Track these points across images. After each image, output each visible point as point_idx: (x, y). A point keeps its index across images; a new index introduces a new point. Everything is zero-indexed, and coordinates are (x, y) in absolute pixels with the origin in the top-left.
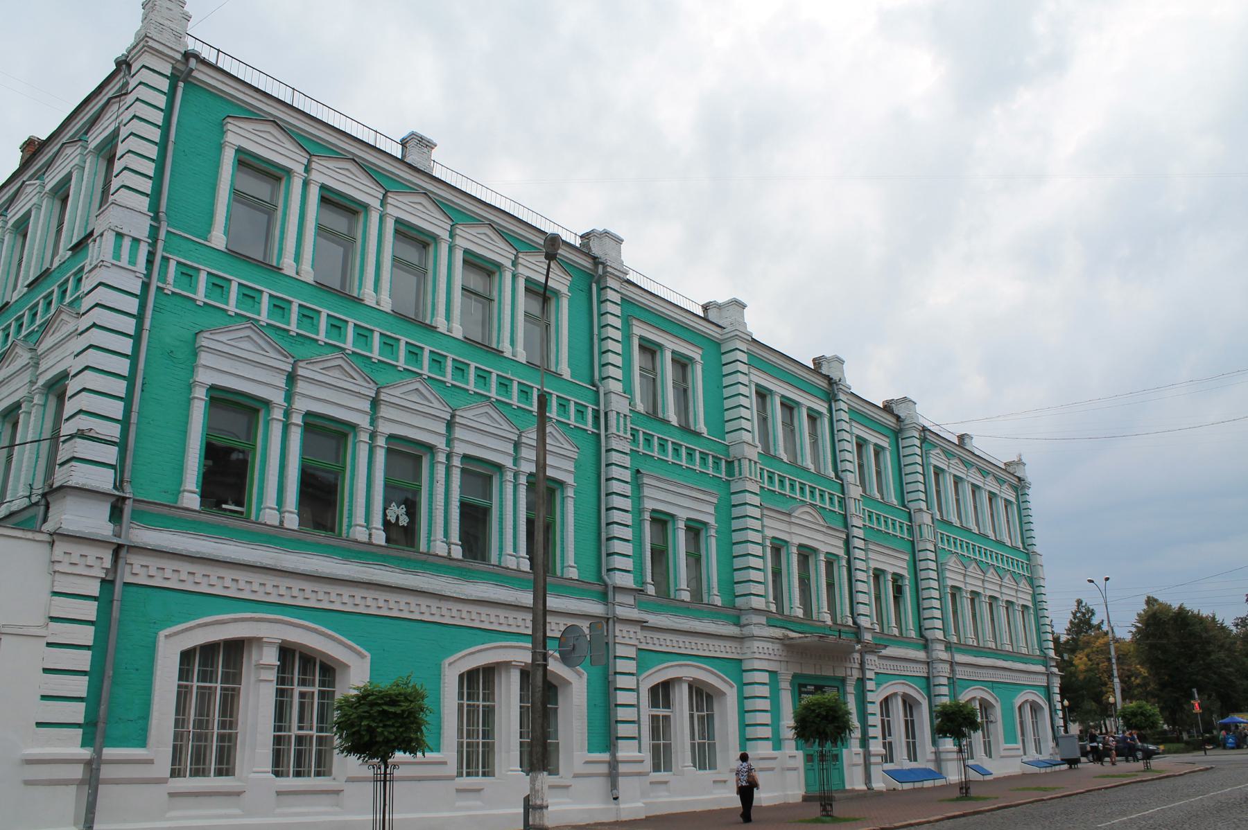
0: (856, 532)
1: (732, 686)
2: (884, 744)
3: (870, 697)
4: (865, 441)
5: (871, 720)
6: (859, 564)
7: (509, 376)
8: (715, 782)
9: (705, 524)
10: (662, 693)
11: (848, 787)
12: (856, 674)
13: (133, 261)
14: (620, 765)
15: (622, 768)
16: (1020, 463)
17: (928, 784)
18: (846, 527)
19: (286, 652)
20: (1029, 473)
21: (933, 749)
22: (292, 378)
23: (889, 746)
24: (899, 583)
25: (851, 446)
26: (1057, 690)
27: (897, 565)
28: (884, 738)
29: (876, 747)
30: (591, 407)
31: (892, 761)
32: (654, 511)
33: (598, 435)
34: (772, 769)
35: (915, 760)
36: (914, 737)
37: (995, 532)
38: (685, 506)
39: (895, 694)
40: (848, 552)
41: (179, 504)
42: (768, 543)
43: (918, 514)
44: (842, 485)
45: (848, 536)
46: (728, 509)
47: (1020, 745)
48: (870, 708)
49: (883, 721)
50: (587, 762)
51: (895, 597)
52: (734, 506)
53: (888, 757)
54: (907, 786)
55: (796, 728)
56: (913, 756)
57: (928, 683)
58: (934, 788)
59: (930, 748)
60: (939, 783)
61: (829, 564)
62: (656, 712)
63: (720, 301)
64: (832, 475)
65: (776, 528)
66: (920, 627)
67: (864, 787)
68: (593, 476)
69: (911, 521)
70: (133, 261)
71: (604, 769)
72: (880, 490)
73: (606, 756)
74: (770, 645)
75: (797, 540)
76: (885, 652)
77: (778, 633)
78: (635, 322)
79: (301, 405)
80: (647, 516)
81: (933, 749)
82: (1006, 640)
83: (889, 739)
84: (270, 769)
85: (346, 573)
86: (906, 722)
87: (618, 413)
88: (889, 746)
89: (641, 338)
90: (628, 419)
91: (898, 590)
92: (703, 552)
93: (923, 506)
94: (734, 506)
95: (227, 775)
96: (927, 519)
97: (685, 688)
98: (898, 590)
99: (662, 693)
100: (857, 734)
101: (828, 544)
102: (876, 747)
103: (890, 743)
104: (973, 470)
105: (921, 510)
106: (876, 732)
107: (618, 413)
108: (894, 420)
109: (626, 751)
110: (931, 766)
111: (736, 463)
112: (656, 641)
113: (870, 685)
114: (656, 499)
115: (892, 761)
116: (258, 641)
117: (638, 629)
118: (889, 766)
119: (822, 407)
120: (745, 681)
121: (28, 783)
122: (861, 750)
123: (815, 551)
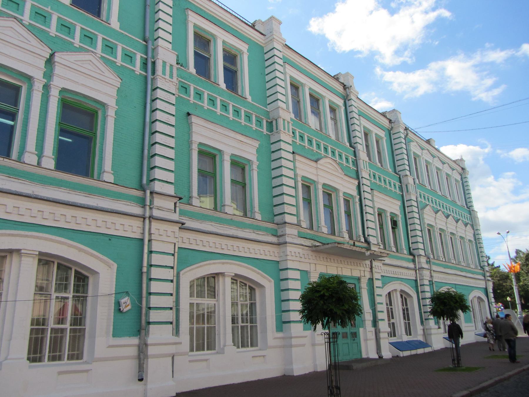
0: (365, 181)
1: (270, 281)
2: (389, 324)
3: (377, 291)
4: (370, 130)
5: (379, 308)
6: (368, 203)
7: (49, 9)
8: (253, 357)
9: (249, 161)
10: (208, 285)
11: (364, 356)
12: (368, 276)
13: (171, 76)
14: (150, 348)
15: (151, 350)
16: (462, 160)
17: (420, 351)
18: (358, 178)
19: (45, 260)
20: (467, 165)
21: (422, 328)
22: (50, 61)
23: (393, 326)
24: (395, 219)
25: (435, 171)
26: (491, 291)
27: (393, 207)
28: (389, 320)
29: (384, 326)
30: (139, 57)
31: (395, 336)
32: (200, 144)
33: (146, 77)
34: (303, 345)
35: (410, 335)
36: (409, 320)
37: (430, 184)
38: (232, 145)
39: (395, 290)
40: (360, 194)
41: (100, 179)
42: (299, 179)
43: (405, 178)
44: (355, 152)
45: (359, 183)
46: (270, 152)
47: (474, 324)
48: (378, 299)
49: (388, 308)
50: (110, 346)
51: (393, 228)
52: (273, 152)
53: (393, 334)
54: (407, 353)
55: (302, 312)
56: (408, 332)
57: (416, 284)
58: (424, 354)
59: (419, 327)
60: (427, 350)
61: (347, 202)
62: (196, 300)
63: (263, 21)
64: (348, 144)
65: (306, 169)
66: (410, 248)
67: (376, 356)
68: (140, 108)
69: (400, 182)
70: (171, 76)
71: (133, 352)
72: (380, 161)
73: (135, 341)
74: (300, 250)
75: (322, 181)
76: (387, 261)
77: (308, 243)
78: (190, 13)
79: (58, 83)
80: (195, 147)
81: (422, 328)
82: (441, 254)
83: (392, 321)
84: (25, 356)
85: (199, 227)
86: (403, 310)
87: (284, 120)
88: (393, 326)
89: (195, 26)
90: (290, 124)
91: (394, 224)
92: (247, 181)
93: (408, 173)
94: (273, 152)
95: (78, 359)
96: (410, 180)
97: (228, 280)
98: (394, 224)
99: (208, 285)
100: (368, 316)
101: (346, 186)
102: (384, 326)
103: (393, 324)
104: (436, 159)
105: (406, 175)
106: (382, 316)
107: (284, 120)
108: (387, 122)
109: (158, 335)
110: (421, 338)
111: (274, 122)
112: (252, 251)
113: (377, 283)
114: (204, 133)
115: (395, 336)
116: (222, 274)
117: (176, 228)
118: (394, 340)
119: (340, 102)
120: (281, 278)
121: (190, 361)
122: (373, 329)
123: (336, 190)
